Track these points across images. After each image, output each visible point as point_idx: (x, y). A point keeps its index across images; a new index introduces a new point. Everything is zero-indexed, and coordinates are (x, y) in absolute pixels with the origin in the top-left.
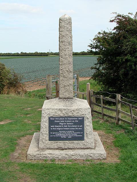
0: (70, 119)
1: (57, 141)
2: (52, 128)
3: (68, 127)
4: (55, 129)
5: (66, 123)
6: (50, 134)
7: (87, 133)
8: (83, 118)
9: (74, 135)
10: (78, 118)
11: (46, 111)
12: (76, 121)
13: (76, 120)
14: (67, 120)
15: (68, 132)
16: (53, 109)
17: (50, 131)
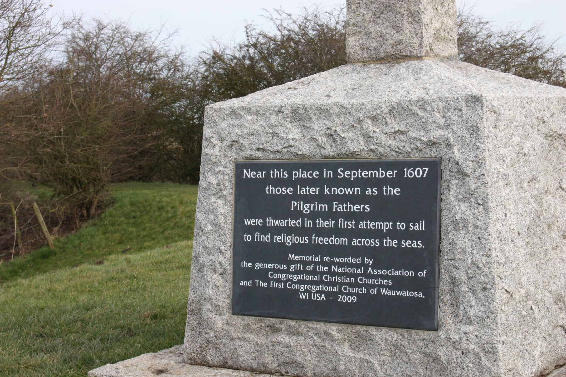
0: (354, 174)
1: (273, 320)
2: (251, 230)
3: (337, 232)
4: (266, 238)
5: (329, 200)
6: (239, 274)
7: (453, 281)
8: (435, 166)
9: (373, 286)
10: (399, 166)
11: (224, 125)
12: (388, 190)
13: (386, 181)
14: (336, 182)
15: (340, 265)
16: (257, 113)
17: (242, 250)
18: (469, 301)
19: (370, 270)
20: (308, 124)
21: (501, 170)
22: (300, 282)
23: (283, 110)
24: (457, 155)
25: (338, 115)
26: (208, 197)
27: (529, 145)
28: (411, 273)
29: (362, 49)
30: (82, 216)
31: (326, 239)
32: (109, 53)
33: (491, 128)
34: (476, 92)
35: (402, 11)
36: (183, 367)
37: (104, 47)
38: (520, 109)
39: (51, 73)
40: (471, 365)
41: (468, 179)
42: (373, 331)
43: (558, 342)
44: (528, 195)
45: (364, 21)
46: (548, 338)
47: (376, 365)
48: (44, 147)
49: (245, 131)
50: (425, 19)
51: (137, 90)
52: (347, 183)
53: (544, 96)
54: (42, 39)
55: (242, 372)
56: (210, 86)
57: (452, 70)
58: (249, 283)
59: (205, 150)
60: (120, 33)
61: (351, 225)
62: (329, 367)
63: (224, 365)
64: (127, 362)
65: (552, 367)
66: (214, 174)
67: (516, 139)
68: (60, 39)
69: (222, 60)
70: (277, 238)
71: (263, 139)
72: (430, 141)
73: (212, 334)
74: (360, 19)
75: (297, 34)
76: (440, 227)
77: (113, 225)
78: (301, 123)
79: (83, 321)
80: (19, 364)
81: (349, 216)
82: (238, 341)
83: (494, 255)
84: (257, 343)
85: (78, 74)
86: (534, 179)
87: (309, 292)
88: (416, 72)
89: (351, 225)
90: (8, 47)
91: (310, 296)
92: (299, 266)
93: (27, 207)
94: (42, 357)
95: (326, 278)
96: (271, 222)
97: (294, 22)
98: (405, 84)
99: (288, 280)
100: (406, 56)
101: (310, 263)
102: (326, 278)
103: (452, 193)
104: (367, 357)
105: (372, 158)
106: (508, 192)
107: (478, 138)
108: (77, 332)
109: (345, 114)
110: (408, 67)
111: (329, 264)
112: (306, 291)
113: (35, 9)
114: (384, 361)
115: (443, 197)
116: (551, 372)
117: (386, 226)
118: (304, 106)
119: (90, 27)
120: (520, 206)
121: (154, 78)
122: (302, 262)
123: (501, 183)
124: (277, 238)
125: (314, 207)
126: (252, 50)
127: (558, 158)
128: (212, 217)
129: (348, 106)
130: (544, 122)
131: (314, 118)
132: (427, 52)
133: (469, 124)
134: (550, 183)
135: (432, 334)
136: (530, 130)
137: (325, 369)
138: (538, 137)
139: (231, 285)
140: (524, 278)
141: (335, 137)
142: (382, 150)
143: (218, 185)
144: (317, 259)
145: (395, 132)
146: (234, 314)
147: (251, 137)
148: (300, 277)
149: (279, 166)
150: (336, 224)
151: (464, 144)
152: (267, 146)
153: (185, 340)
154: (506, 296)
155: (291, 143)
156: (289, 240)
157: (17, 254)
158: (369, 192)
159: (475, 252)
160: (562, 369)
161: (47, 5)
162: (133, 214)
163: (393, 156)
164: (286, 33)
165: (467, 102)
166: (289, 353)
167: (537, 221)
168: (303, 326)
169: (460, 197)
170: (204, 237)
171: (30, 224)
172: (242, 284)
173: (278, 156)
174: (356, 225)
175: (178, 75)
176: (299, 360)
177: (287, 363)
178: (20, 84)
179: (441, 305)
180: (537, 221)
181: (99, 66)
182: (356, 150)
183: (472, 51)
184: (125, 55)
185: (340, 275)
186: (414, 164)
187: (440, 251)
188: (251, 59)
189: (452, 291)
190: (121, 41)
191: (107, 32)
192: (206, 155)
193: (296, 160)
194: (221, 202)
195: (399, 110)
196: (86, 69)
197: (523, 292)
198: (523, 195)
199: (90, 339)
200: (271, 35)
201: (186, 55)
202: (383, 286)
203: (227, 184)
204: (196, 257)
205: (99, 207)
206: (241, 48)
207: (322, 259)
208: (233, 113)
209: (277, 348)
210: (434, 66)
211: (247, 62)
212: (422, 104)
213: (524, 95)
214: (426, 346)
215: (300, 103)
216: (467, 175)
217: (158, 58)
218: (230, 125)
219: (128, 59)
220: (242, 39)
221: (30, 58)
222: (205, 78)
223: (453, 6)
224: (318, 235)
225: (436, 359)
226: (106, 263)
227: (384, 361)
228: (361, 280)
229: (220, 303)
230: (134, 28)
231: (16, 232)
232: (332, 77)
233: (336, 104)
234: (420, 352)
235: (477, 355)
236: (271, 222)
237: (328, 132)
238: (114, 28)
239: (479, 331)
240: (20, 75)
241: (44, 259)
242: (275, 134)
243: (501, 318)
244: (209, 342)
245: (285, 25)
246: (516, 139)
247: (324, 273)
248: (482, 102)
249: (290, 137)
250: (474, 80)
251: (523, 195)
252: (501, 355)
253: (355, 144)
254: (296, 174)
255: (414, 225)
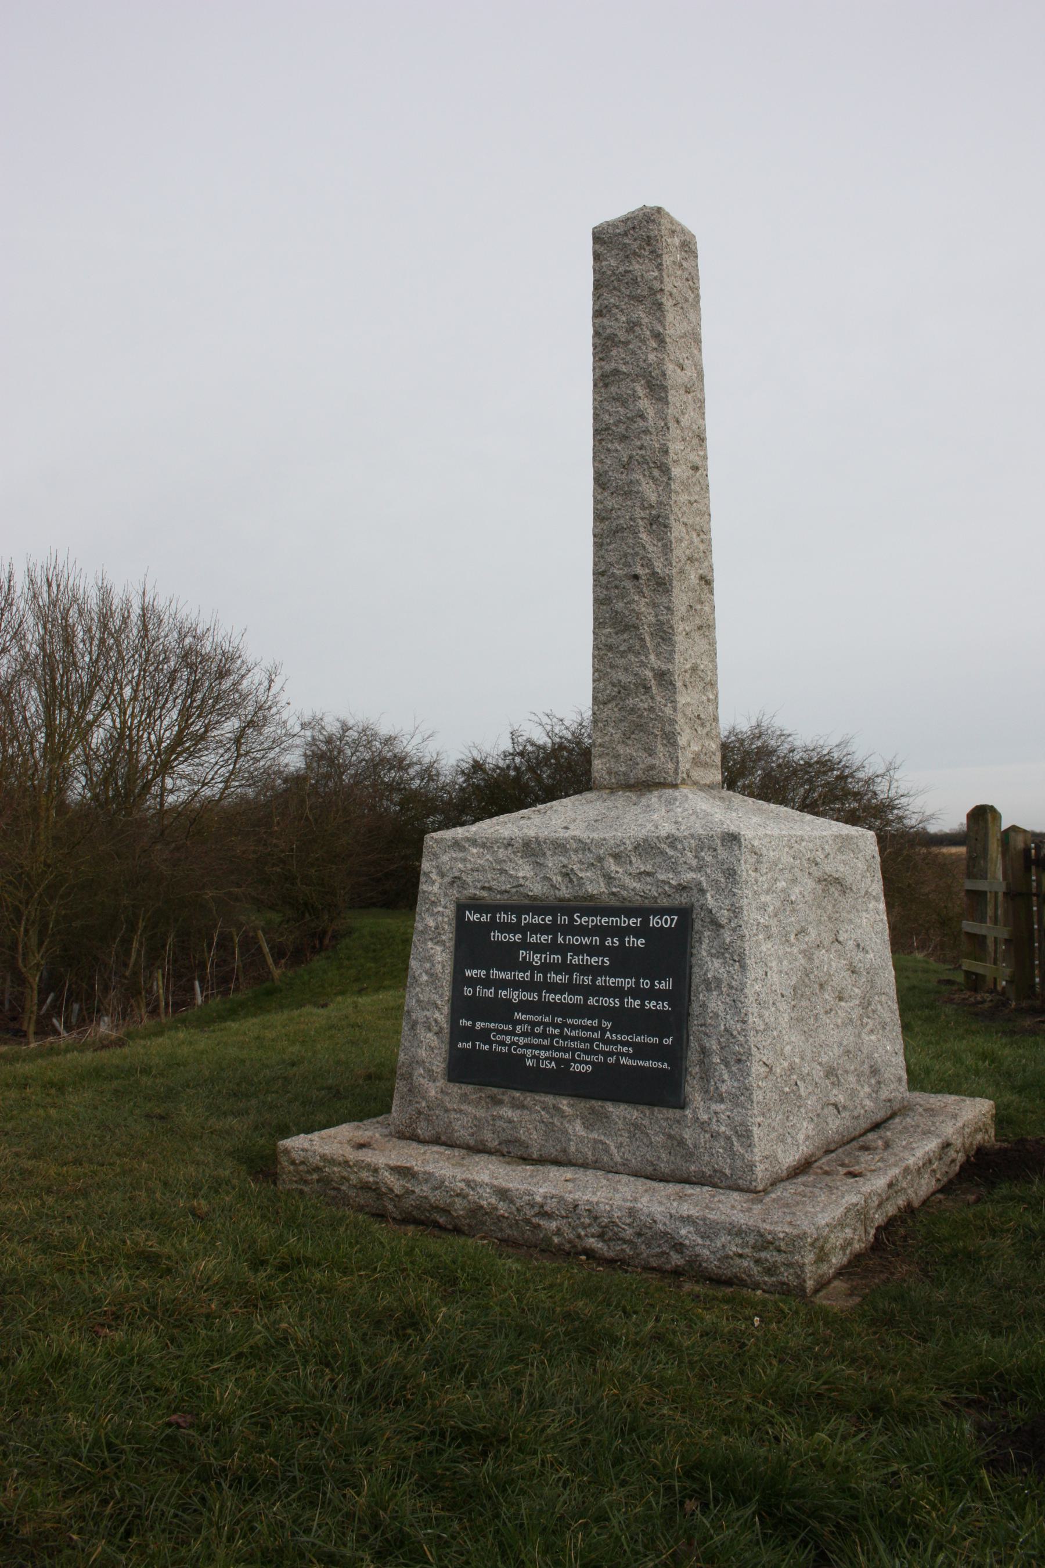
1: (495, 1090)
2: (473, 982)
3: (571, 988)
4: (489, 993)
6: (457, 1034)
7: (704, 1051)
9: (611, 1054)
10: (643, 912)
11: (445, 858)
12: (631, 941)
13: (629, 931)
14: (572, 929)
15: (573, 1027)
16: (484, 846)
18: (721, 1075)
19: (608, 1034)
20: (541, 860)
21: (762, 921)
22: (527, 1046)
23: (513, 842)
24: (710, 900)
25: (576, 851)
26: (425, 942)
27: (797, 891)
28: (655, 1040)
29: (609, 773)
30: (314, 947)
31: (558, 996)
32: (354, 758)
33: (750, 872)
34: (733, 829)
35: (655, 731)
36: (389, 1141)
37: (349, 752)
38: (787, 849)
39: (285, 781)
40: (721, 1151)
41: (722, 931)
42: (610, 1107)
43: (827, 1124)
44: (795, 950)
45: (611, 741)
46: (815, 1119)
47: (612, 1148)
48: (274, 865)
49: (469, 866)
50: (682, 741)
51: (385, 803)
52: (583, 931)
53: (816, 833)
54: (277, 742)
55: (456, 1150)
56: (468, 799)
57: (711, 801)
58: (468, 1045)
59: (423, 887)
60: (368, 736)
61: (587, 980)
62: (558, 1147)
63: (436, 1141)
64: (325, 1133)
65: (819, 1153)
66: (432, 915)
67: (781, 884)
68: (298, 741)
69: (484, 771)
70: (503, 994)
71: (489, 876)
72: (680, 885)
73: (424, 1104)
74: (607, 738)
75: (569, 741)
76: (690, 986)
77: (349, 959)
78: (533, 859)
79: (285, 1078)
80: (203, 1128)
81: (585, 970)
82: (453, 1113)
83: (750, 1021)
84: (475, 1116)
85: (317, 781)
86: (803, 931)
87: (537, 1058)
88: (671, 801)
89: (587, 980)
90: (238, 750)
91: (538, 1063)
92: (526, 1027)
93: (251, 934)
94: (232, 1121)
95: (557, 1042)
96: (496, 974)
97: (567, 728)
98: (655, 817)
99: (513, 1043)
100: (660, 783)
101: (539, 1024)
102: (557, 1042)
103: (704, 946)
104: (602, 1138)
105: (614, 902)
106: (769, 946)
107: (735, 883)
108: (277, 1092)
109: (584, 850)
110: (661, 796)
111: (561, 1026)
112: (534, 1057)
113: (270, 708)
114: (621, 1144)
115: (694, 951)
116: (819, 1159)
117: (628, 983)
118: (537, 838)
119: (332, 727)
120: (785, 962)
121: (405, 788)
122: (530, 1023)
123: (761, 937)
124: (503, 994)
125: (546, 958)
126: (518, 760)
127: (834, 906)
128: (428, 965)
129: (588, 841)
130: (817, 864)
131: (549, 853)
132: (684, 779)
133: (725, 867)
134: (823, 935)
135: (678, 1113)
136: (798, 874)
137: (553, 1150)
138: (809, 881)
139: (447, 1047)
140: (788, 1048)
141: (572, 876)
142: (624, 893)
143: (437, 928)
144: (547, 1020)
145: (640, 873)
146: (449, 1080)
147: (476, 874)
148: (527, 1040)
149: (506, 908)
150: (570, 979)
151: (719, 890)
152: (494, 884)
153: (393, 1109)
154: (763, 1070)
155: (521, 881)
156: (516, 996)
157: (237, 989)
158: (608, 942)
159: (728, 1017)
160: (833, 1155)
161: (283, 703)
162: (372, 946)
163: (638, 901)
164: (558, 740)
165: (723, 840)
166: (512, 1129)
167: (807, 981)
168: (529, 1099)
169: (713, 951)
170: (418, 989)
171: (253, 954)
172: (460, 1045)
173: (506, 896)
174: (594, 981)
175: (432, 785)
176: (523, 1138)
177: (510, 1141)
178: (251, 792)
179: (688, 1078)
180: (807, 981)
181: (343, 773)
182: (595, 892)
183: (772, 768)
184: (372, 760)
185: (574, 1039)
186: (661, 912)
187: (689, 1014)
188: (517, 769)
189: (702, 1062)
190: (369, 744)
191: (353, 734)
192: (424, 892)
193: (526, 902)
194: (439, 948)
195: (646, 848)
196: (328, 776)
197: (786, 1064)
198: (788, 950)
199: (290, 1102)
200: (541, 742)
201: (443, 762)
202: (623, 1054)
203: (446, 927)
204: (408, 1012)
205: (334, 937)
206: (505, 756)
207: (553, 1020)
208: (457, 844)
209: (499, 1123)
210: (690, 796)
211: (513, 773)
212: (672, 841)
213: (793, 832)
214: (671, 1127)
215: (533, 835)
216: (721, 926)
217: (410, 765)
218: (452, 859)
219: (375, 766)
220: (507, 745)
221: (262, 763)
222: (462, 789)
223: (717, 726)
224: (549, 992)
225: (681, 1143)
226: (332, 1006)
227: (621, 1144)
228: (598, 1046)
229: (434, 1068)
230: (384, 730)
231: (237, 963)
232: (574, 805)
233: (573, 838)
234: (663, 1134)
235: (728, 1138)
236: (496, 974)
237: (564, 870)
238: (360, 730)
239: (731, 1111)
240: (251, 782)
241: (268, 997)
242: (503, 871)
243: (758, 1096)
244: (420, 1113)
245: (556, 731)
246: (781, 884)
247: (555, 1036)
248: (739, 842)
249: (521, 874)
250: (734, 814)
251: (788, 950)
252: (756, 1140)
253: (595, 886)
254: (525, 919)
255: (660, 983)
